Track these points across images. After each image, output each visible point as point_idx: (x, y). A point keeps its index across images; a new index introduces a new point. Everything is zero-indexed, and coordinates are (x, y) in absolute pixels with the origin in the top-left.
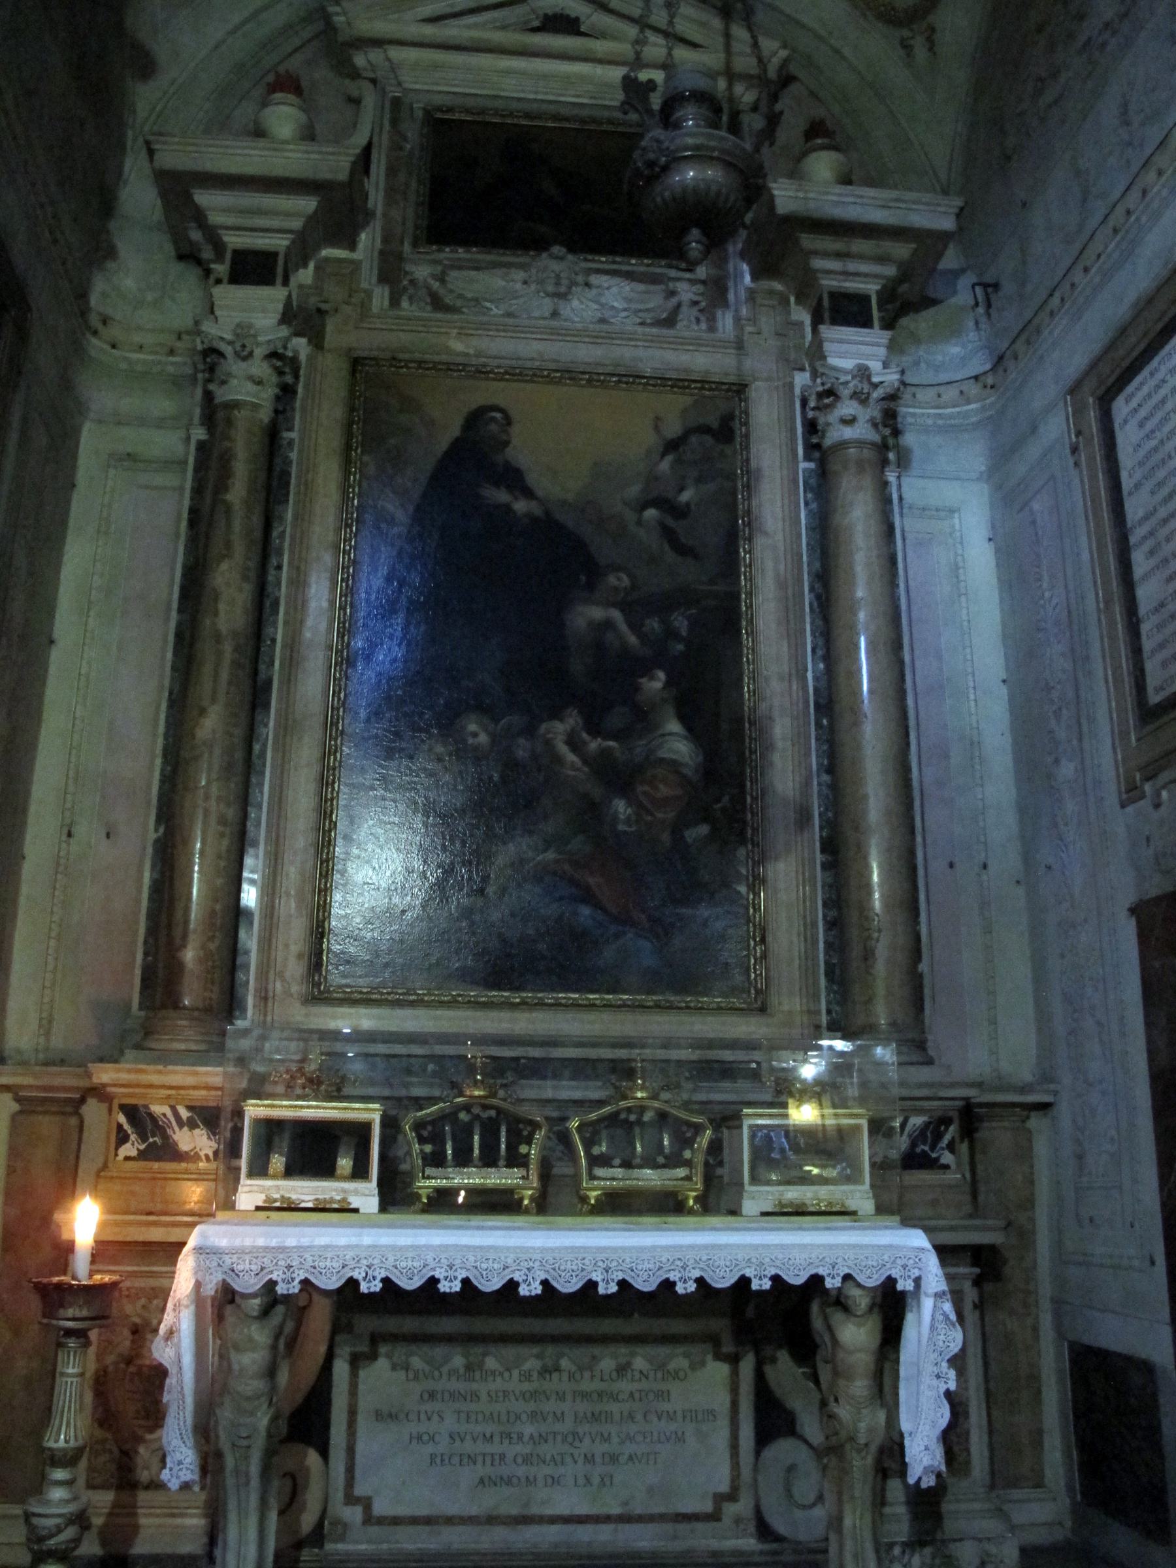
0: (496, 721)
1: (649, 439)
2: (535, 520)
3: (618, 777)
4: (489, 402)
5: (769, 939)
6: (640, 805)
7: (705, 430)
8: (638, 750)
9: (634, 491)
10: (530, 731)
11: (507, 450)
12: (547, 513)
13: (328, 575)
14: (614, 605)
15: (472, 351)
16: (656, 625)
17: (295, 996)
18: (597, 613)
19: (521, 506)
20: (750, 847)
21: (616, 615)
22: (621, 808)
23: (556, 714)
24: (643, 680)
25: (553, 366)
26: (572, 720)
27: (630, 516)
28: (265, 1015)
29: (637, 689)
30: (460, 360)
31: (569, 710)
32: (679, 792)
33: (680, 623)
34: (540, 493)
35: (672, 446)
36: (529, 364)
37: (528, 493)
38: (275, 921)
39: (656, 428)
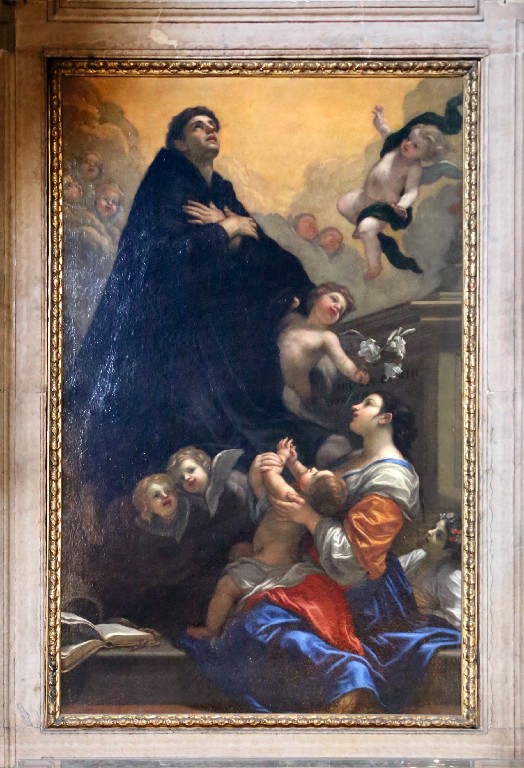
0: (212, 455)
1: (373, 138)
2: (246, 239)
3: (334, 507)
4: (193, 104)
5: (483, 660)
6: (355, 532)
7: (426, 119)
8: (353, 478)
9: (352, 198)
10: (244, 465)
11: (216, 161)
12: (259, 230)
13: (39, 313)
14: (331, 328)
15: (175, 43)
16: (372, 347)
17: (35, 725)
18: (311, 338)
19: (232, 225)
20: (466, 571)
21: (332, 339)
22: (336, 536)
23: (272, 447)
24: (359, 407)
25: (264, 54)
26: (287, 450)
27: (347, 228)
28: (9, 744)
29: (352, 415)
30: (164, 55)
31: (284, 442)
32: (392, 518)
33: (398, 344)
34: (250, 207)
35: (393, 142)
36: (237, 54)
37: (240, 210)
38: (12, 658)
39: (376, 122)
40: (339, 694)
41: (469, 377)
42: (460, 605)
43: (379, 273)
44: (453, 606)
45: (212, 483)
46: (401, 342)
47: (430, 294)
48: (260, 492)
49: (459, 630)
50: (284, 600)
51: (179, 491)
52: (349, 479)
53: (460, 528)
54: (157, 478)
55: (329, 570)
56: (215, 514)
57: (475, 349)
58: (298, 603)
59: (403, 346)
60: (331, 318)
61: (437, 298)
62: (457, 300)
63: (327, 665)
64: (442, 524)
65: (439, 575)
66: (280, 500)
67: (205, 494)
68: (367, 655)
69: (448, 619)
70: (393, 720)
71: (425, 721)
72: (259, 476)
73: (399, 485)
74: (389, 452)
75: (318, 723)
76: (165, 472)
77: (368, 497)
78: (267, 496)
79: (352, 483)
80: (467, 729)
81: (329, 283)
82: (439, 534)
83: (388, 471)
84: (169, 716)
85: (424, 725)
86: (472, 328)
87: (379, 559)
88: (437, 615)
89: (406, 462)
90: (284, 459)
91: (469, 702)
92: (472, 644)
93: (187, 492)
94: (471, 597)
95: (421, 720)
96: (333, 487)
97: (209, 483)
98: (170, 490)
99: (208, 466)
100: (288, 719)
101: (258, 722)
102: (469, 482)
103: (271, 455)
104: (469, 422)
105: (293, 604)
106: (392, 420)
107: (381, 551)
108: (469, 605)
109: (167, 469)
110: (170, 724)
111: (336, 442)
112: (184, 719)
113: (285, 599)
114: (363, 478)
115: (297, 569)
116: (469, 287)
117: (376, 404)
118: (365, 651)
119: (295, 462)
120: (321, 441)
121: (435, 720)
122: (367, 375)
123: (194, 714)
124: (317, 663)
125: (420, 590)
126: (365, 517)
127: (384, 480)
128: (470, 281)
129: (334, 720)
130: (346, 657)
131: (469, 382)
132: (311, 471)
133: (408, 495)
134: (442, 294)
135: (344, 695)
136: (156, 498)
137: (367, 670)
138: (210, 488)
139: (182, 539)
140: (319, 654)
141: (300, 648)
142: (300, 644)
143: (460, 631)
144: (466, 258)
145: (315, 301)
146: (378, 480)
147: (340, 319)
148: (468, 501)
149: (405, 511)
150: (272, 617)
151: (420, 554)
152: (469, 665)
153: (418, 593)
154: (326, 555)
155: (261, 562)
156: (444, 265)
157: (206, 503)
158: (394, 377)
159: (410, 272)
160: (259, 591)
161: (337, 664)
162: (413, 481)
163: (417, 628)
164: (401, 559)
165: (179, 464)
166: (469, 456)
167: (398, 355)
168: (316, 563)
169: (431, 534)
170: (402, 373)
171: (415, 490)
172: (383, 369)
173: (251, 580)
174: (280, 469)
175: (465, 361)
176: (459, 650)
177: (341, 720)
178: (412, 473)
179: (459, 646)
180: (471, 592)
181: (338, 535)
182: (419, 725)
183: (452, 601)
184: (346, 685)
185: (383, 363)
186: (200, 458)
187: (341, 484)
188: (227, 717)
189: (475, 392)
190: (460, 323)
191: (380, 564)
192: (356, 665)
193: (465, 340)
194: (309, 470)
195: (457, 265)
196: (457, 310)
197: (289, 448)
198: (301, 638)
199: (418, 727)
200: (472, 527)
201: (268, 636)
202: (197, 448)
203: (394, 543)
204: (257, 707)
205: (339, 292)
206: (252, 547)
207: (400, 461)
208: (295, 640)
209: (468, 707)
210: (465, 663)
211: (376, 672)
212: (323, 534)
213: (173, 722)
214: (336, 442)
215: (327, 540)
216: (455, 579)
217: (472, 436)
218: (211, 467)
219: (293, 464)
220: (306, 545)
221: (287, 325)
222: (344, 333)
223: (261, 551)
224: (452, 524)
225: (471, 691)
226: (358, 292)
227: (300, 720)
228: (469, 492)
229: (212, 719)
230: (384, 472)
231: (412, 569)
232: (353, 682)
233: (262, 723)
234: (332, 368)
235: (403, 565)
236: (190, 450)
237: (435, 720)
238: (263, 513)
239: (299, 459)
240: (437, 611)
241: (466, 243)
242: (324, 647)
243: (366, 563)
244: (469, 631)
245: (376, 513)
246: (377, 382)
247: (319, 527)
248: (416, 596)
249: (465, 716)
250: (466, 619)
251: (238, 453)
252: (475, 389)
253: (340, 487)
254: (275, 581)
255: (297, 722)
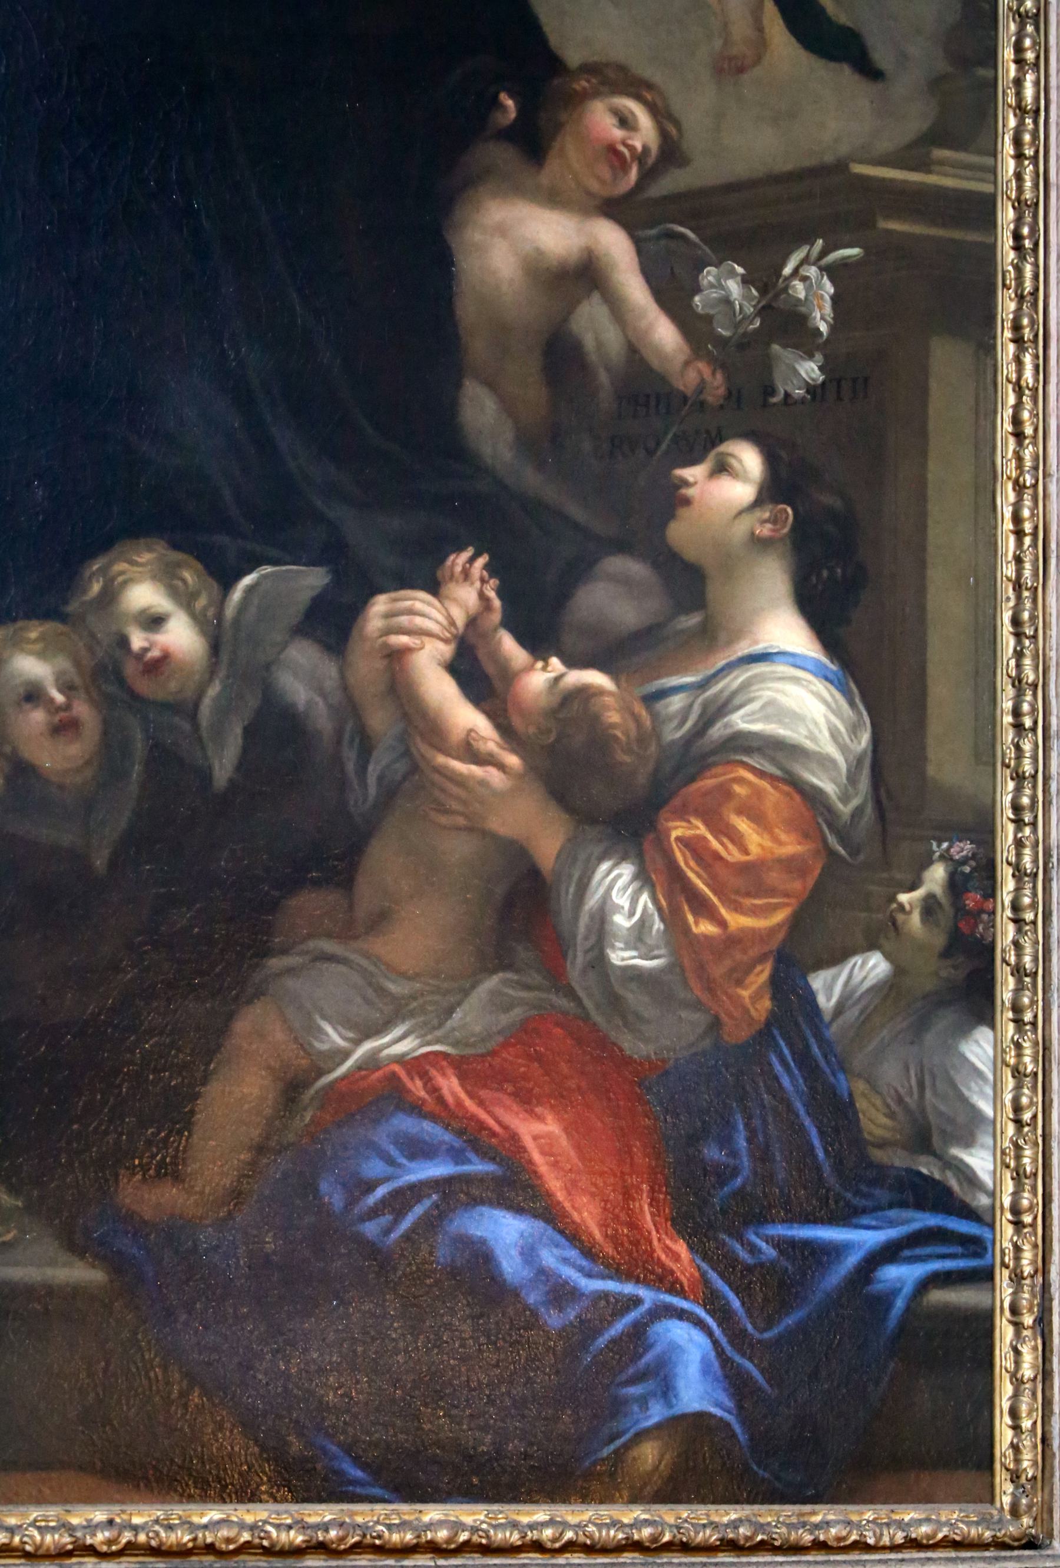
0: (227, 580)
3: (620, 793)
8: (676, 703)
10: (332, 622)
14: (613, 209)
16: (734, 287)
18: (553, 232)
21: (613, 242)
22: (619, 893)
24: (694, 473)
26: (469, 589)
29: (673, 499)
32: (791, 846)
33: (814, 292)
40: (624, 1433)
41: (1016, 421)
42: (991, 1142)
43: (758, 60)
44: (968, 1142)
45: (222, 673)
46: (820, 286)
47: (910, 146)
48: (380, 720)
49: (986, 1219)
50: (450, 1099)
51: (111, 689)
52: (659, 706)
53: (991, 891)
54: (33, 635)
55: (598, 1006)
56: (231, 780)
57: (1036, 336)
58: (499, 1111)
59: (827, 298)
60: (615, 178)
61: (924, 165)
62: (983, 180)
63: (587, 1329)
64: (937, 875)
65: (930, 1038)
66: (448, 754)
67: (196, 705)
68: (713, 1301)
69: (954, 1183)
70: (791, 1526)
71: (888, 1525)
72: (380, 664)
73: (812, 738)
74: (785, 631)
75: (554, 1540)
76: (62, 618)
77: (719, 770)
78: (404, 738)
79: (670, 718)
80: (1016, 1553)
81: (607, 65)
82: (929, 906)
83: (777, 691)
84: (35, 1513)
85: (886, 1541)
86: (1028, 270)
87: (751, 978)
88: (925, 1171)
89: (833, 667)
90: (460, 618)
91: (1017, 1461)
92: (1027, 1270)
93: (134, 696)
94: (1027, 1116)
95: (874, 1521)
96: (613, 726)
97: (212, 670)
98: (78, 681)
99: (210, 613)
100: (458, 1526)
101: (357, 1539)
102: (1018, 748)
103: (420, 600)
104: (1019, 560)
105: (483, 1115)
106: (793, 529)
107: (754, 952)
108: (1021, 1142)
109: (73, 607)
110: (38, 1548)
111: (625, 581)
112: (92, 1527)
113: (454, 1094)
114: (705, 706)
115: (494, 993)
116: (1017, 142)
117: (745, 471)
118: (706, 1282)
119: (495, 630)
120: (579, 570)
121: (919, 1522)
122: (719, 376)
123: (129, 1508)
124: (554, 1319)
125: (874, 1087)
126: (710, 837)
127: (767, 719)
128: (1021, 124)
129: (608, 1526)
130: (647, 1305)
131: (1019, 436)
132: (544, 669)
133: (840, 774)
134: (941, 153)
135: (641, 1436)
136: (27, 706)
137: (713, 1354)
138: (214, 690)
139: (113, 864)
140: (562, 1294)
141: (498, 1266)
142: (499, 1252)
143: (992, 1226)
144: (1008, 53)
145: (563, 116)
146: (751, 718)
147: (639, 186)
148: (1017, 808)
149: (830, 826)
150: (412, 1157)
151: (873, 967)
152: (1018, 1334)
153: (864, 1095)
154: (586, 952)
155: (377, 960)
156: (942, 66)
157: (200, 739)
158: (799, 392)
159: (847, 69)
160: (372, 1062)
161: (619, 1326)
162: (854, 730)
163: (864, 1211)
164: (818, 981)
165: (110, 596)
166: (1019, 666)
167: (810, 325)
168: (555, 975)
169: (907, 907)
170: (824, 383)
171: (860, 761)
172: (767, 364)
173: (344, 1022)
174: (447, 651)
175: (1008, 370)
176: (989, 1285)
177: (631, 1526)
178: (852, 704)
179: (985, 1277)
180: (1025, 1100)
181: (625, 888)
182: (871, 1541)
183: (968, 1126)
184: (643, 1402)
185: (768, 345)
186: (184, 581)
187: (636, 719)
188: (249, 1519)
189: (1036, 468)
190: (990, 251)
191: (753, 995)
192: (678, 1332)
193: (1007, 305)
194: (540, 664)
195: (982, 72)
196: (983, 211)
197: (478, 584)
198: (504, 1231)
199: (867, 1548)
200: (1028, 892)
201: (396, 1222)
202: (176, 546)
203: (796, 924)
204: (355, 1482)
205: (638, 98)
206: (351, 907)
207: (817, 662)
208: (483, 1241)
209: (1015, 1476)
210: (1004, 1332)
211: (738, 1359)
212: (580, 879)
213: (48, 1538)
214: (625, 581)
215: (592, 901)
216: (977, 1056)
217: (1028, 605)
218: (220, 615)
219: (487, 637)
220: (525, 913)
221: (470, 182)
222: (653, 232)
223: (380, 921)
224: (968, 877)
225: (1026, 1424)
226: (697, 106)
227: (495, 1527)
228: (1019, 777)
229: (192, 1527)
230: (766, 693)
231: (852, 1015)
232: (667, 1390)
233: (368, 1540)
234: (612, 338)
235: (821, 1000)
236: (150, 550)
237: (919, 1522)
238: (390, 793)
239: (510, 623)
240: (923, 1159)
241: (1010, 9)
242: (574, 1266)
243: (710, 987)
244: (1018, 1224)
245: (743, 825)
246: (747, 405)
247: (568, 854)
248: (861, 1104)
249: (1007, 1507)
250: (1009, 1186)
251: (311, 580)
252: (1036, 458)
253: (632, 726)
254: (424, 1031)
255: (488, 1537)
